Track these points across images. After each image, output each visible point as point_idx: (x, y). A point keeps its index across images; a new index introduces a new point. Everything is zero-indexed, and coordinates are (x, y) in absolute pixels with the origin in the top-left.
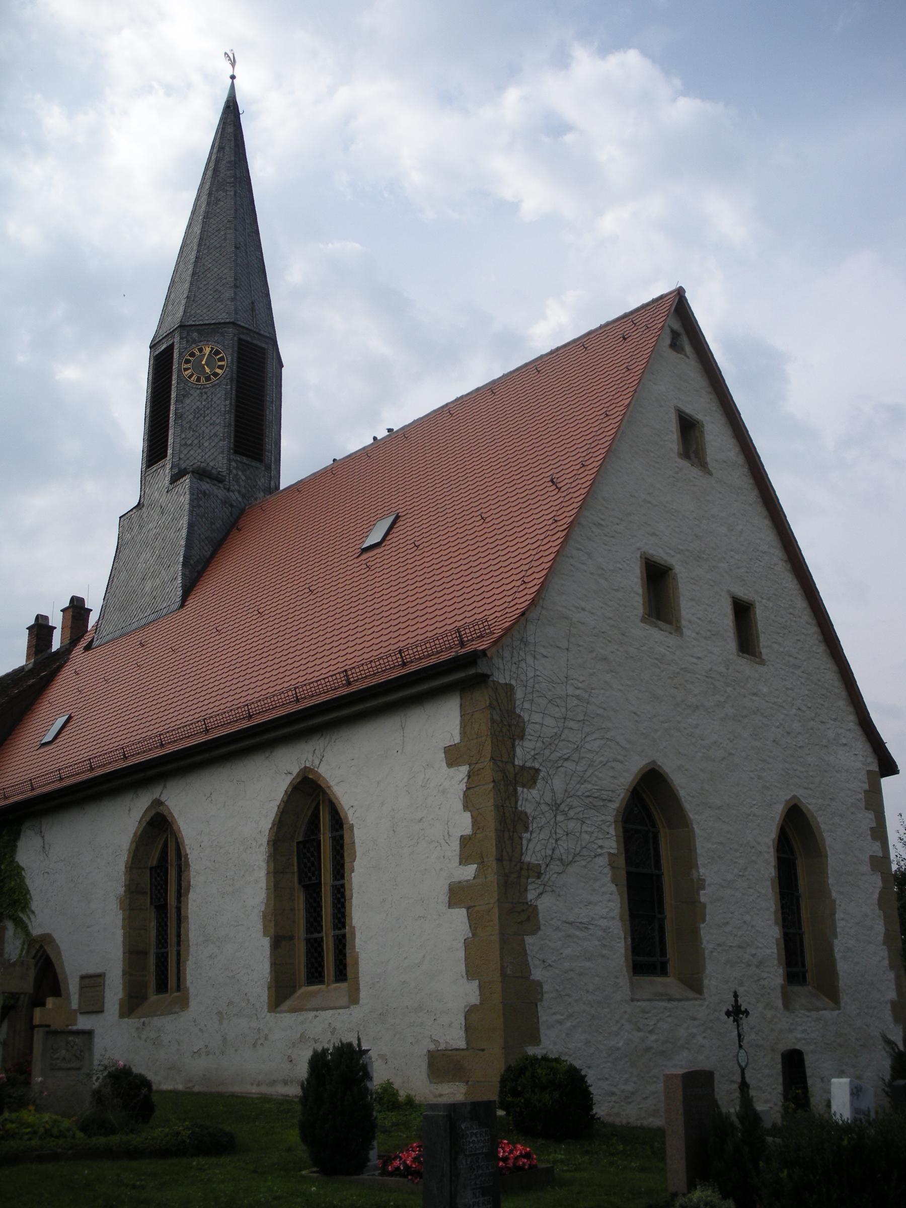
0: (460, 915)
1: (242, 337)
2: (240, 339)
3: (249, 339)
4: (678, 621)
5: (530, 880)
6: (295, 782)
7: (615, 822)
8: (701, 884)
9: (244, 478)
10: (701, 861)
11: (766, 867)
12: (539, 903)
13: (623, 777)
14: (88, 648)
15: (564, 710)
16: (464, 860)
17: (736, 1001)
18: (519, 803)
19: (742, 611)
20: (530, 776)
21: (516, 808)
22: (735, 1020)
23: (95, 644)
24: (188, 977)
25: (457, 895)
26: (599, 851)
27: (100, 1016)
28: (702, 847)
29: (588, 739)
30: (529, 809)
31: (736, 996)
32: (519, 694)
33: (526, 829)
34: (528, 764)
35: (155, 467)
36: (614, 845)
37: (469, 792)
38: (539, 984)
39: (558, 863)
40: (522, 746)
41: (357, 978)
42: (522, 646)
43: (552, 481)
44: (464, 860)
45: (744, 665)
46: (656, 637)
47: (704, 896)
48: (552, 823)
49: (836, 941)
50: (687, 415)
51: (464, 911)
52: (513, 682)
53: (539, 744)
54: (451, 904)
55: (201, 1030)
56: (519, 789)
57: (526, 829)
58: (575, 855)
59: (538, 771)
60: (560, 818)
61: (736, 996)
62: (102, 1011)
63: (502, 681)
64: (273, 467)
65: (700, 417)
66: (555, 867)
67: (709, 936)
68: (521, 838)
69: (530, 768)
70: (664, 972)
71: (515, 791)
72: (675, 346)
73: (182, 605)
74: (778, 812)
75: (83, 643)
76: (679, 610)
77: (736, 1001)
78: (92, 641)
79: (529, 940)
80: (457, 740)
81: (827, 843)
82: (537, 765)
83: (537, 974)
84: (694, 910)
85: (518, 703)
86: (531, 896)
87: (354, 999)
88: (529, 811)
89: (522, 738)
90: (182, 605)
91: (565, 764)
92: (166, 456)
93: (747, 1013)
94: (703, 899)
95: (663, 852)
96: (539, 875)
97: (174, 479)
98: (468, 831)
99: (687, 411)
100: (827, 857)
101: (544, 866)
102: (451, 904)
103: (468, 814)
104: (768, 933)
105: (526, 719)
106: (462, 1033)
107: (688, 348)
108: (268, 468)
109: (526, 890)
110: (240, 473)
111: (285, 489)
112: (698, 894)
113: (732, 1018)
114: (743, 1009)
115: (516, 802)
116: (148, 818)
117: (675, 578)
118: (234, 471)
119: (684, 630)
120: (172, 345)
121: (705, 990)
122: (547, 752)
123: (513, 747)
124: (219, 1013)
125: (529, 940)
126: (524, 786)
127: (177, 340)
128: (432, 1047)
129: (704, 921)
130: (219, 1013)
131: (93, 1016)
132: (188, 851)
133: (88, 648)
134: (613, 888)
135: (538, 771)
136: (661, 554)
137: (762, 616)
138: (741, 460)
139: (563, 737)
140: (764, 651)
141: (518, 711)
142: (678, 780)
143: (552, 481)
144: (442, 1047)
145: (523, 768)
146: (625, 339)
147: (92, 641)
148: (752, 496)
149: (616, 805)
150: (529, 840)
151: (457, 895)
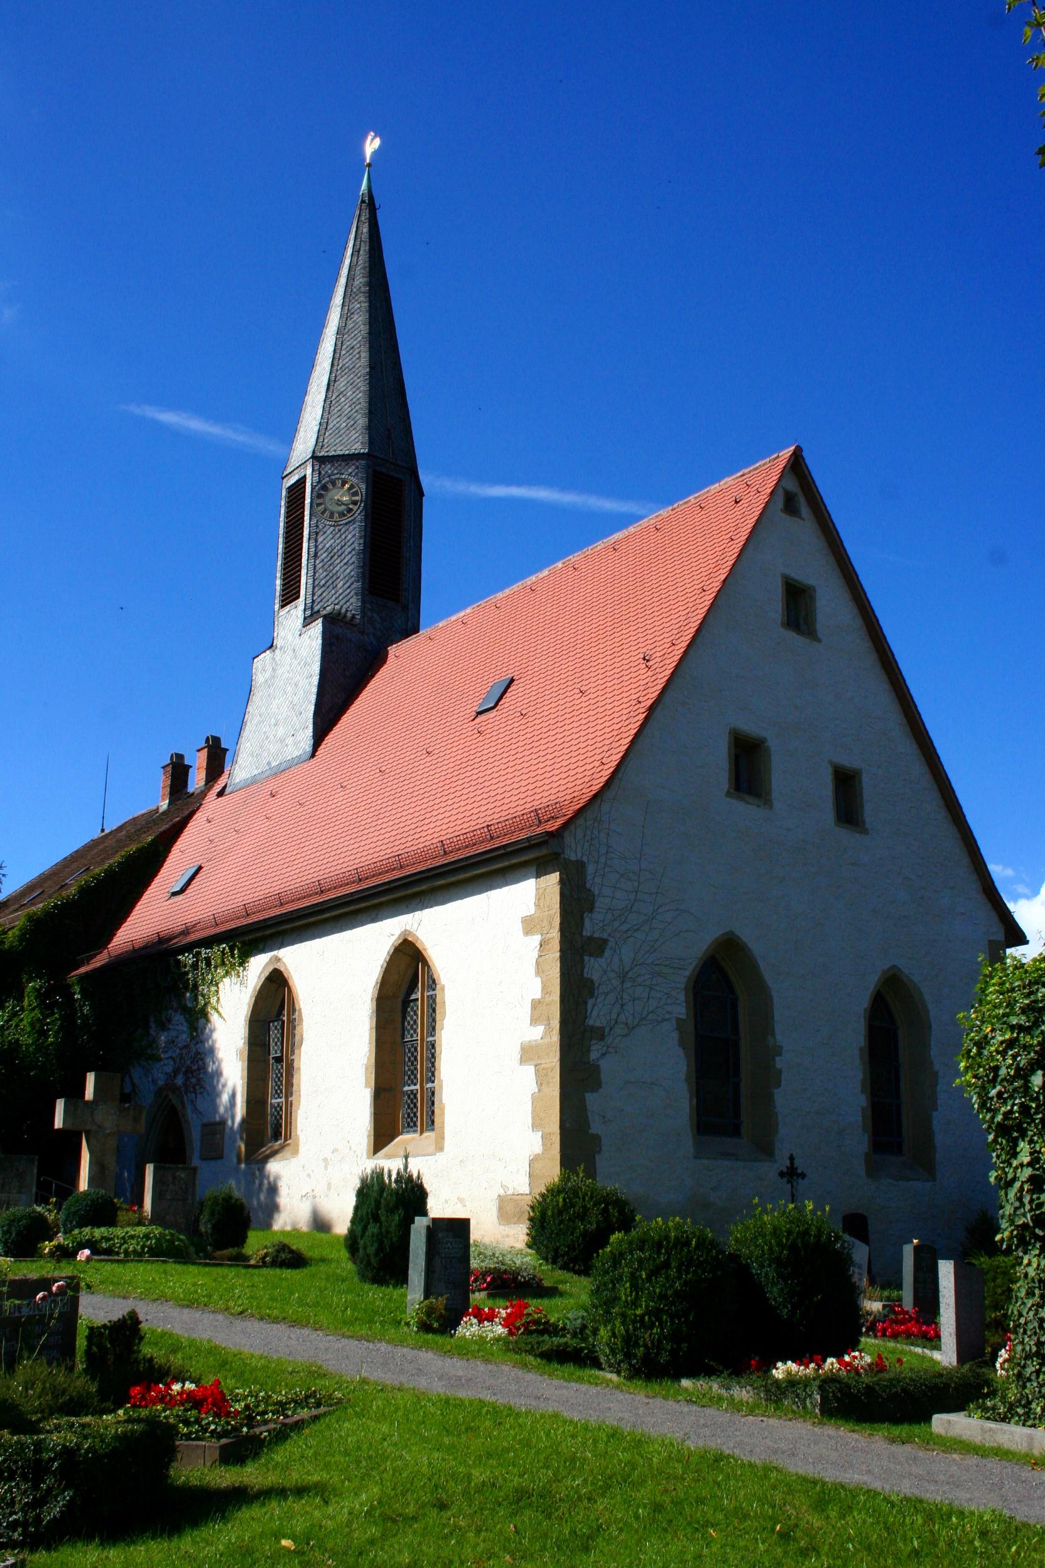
0: (530, 1070)
1: (378, 468)
2: (375, 471)
3: (384, 470)
4: (769, 793)
5: (593, 1042)
6: (397, 944)
7: (686, 988)
8: (778, 1051)
9: (378, 619)
10: (778, 1028)
11: (854, 1035)
12: (601, 1063)
13: (693, 948)
14: (221, 794)
15: (636, 884)
16: (534, 1021)
17: (792, 1163)
18: (586, 970)
19: (846, 782)
20: (598, 947)
21: (582, 975)
22: (788, 1182)
23: (228, 790)
24: (299, 1125)
25: (528, 1053)
26: (667, 1016)
27: (219, 1162)
28: (780, 1013)
29: (660, 910)
30: (595, 977)
31: (792, 1158)
32: (590, 869)
33: (592, 995)
34: (596, 935)
35: (288, 608)
36: (684, 1011)
37: (541, 960)
38: (597, 1139)
39: (623, 1026)
40: (591, 919)
41: (442, 1128)
42: (596, 824)
43: (644, 659)
44: (534, 1021)
45: (845, 835)
46: (744, 810)
47: (779, 1063)
48: (619, 988)
49: (935, 1114)
50: (793, 579)
51: (533, 1068)
52: (585, 859)
53: (609, 916)
54: (523, 1060)
55: (309, 1175)
56: (586, 958)
57: (592, 995)
58: (641, 1020)
59: (605, 941)
60: (628, 984)
61: (792, 1158)
62: (222, 1158)
63: (573, 857)
64: (411, 606)
65: (811, 582)
66: (619, 1030)
67: (783, 1100)
68: (586, 1003)
69: (600, 939)
70: (736, 1132)
71: (583, 961)
72: (790, 507)
73: (313, 755)
74: (872, 981)
75: (217, 788)
76: (770, 783)
77: (792, 1163)
78: (225, 787)
79: (590, 1097)
80: (532, 912)
81: (932, 1014)
82: (605, 936)
83: (596, 1128)
84: (769, 1077)
85: (589, 877)
86: (594, 1055)
87: (440, 1148)
88: (595, 977)
89: (591, 910)
90: (313, 755)
91: (635, 934)
92: (298, 597)
93: (803, 1176)
94: (778, 1065)
95: (741, 1017)
96: (602, 1038)
97: (307, 621)
98: (538, 995)
99: (796, 577)
100: (930, 1027)
101: (607, 1030)
102: (523, 1060)
103: (539, 979)
104: (853, 1101)
105: (596, 893)
106: (527, 1180)
107: (805, 510)
108: (405, 608)
109: (589, 1051)
110: (375, 615)
111: (253, 781)
112: (774, 1060)
113: (785, 1180)
114: (799, 1171)
115: (582, 971)
116: (267, 974)
117: (768, 750)
118: (369, 614)
119: (775, 802)
120: (305, 477)
121: (777, 1152)
122: (616, 924)
123: (582, 918)
124: (325, 1160)
125: (590, 1097)
126: (591, 955)
127: (309, 471)
128: (502, 1192)
129: (779, 1085)
130: (325, 1160)
131: (213, 1163)
132: (302, 1006)
133: (221, 794)
134: (681, 1052)
135: (605, 941)
136: (751, 727)
137: (870, 789)
138: (859, 621)
139: (634, 909)
140: (867, 820)
141: (588, 885)
142: (756, 948)
143: (644, 659)
144: (510, 1192)
145: (590, 938)
146: (737, 502)
147: (225, 787)
148: (871, 660)
149: (687, 973)
150: (594, 1005)
151: (528, 1053)
